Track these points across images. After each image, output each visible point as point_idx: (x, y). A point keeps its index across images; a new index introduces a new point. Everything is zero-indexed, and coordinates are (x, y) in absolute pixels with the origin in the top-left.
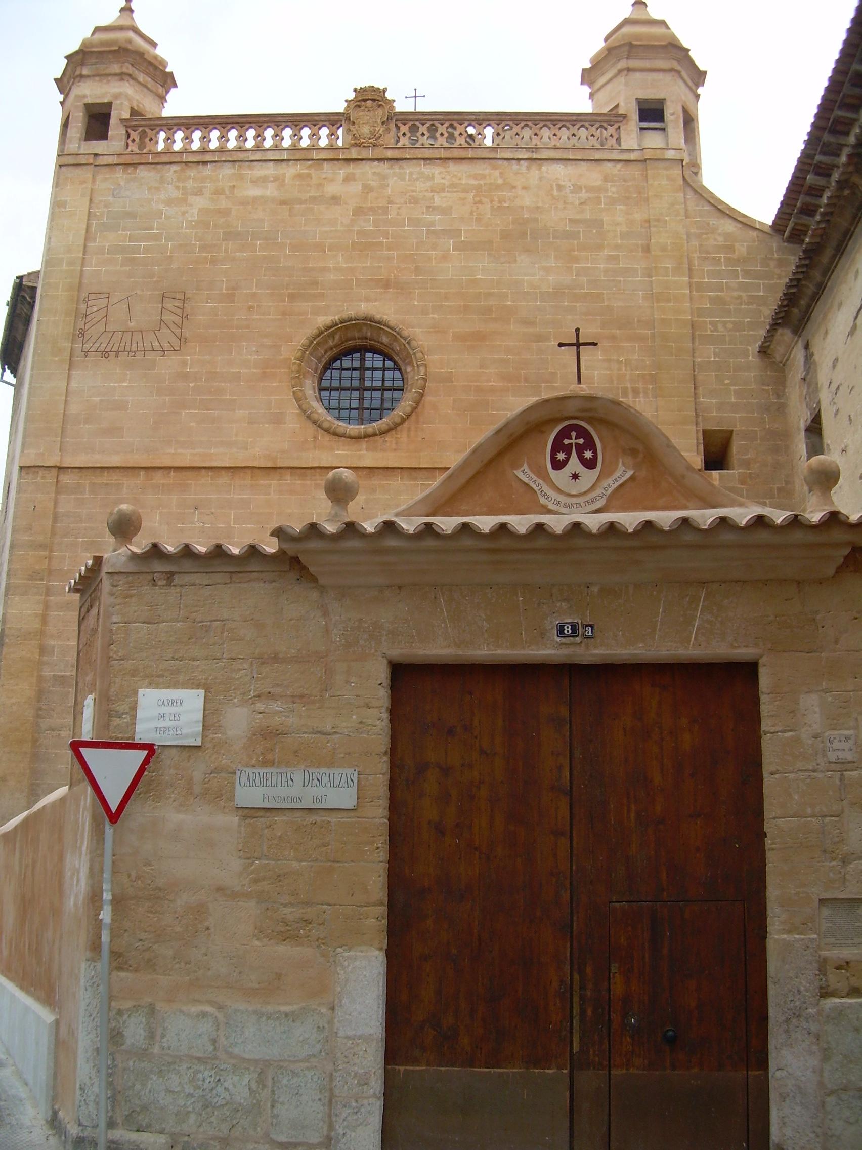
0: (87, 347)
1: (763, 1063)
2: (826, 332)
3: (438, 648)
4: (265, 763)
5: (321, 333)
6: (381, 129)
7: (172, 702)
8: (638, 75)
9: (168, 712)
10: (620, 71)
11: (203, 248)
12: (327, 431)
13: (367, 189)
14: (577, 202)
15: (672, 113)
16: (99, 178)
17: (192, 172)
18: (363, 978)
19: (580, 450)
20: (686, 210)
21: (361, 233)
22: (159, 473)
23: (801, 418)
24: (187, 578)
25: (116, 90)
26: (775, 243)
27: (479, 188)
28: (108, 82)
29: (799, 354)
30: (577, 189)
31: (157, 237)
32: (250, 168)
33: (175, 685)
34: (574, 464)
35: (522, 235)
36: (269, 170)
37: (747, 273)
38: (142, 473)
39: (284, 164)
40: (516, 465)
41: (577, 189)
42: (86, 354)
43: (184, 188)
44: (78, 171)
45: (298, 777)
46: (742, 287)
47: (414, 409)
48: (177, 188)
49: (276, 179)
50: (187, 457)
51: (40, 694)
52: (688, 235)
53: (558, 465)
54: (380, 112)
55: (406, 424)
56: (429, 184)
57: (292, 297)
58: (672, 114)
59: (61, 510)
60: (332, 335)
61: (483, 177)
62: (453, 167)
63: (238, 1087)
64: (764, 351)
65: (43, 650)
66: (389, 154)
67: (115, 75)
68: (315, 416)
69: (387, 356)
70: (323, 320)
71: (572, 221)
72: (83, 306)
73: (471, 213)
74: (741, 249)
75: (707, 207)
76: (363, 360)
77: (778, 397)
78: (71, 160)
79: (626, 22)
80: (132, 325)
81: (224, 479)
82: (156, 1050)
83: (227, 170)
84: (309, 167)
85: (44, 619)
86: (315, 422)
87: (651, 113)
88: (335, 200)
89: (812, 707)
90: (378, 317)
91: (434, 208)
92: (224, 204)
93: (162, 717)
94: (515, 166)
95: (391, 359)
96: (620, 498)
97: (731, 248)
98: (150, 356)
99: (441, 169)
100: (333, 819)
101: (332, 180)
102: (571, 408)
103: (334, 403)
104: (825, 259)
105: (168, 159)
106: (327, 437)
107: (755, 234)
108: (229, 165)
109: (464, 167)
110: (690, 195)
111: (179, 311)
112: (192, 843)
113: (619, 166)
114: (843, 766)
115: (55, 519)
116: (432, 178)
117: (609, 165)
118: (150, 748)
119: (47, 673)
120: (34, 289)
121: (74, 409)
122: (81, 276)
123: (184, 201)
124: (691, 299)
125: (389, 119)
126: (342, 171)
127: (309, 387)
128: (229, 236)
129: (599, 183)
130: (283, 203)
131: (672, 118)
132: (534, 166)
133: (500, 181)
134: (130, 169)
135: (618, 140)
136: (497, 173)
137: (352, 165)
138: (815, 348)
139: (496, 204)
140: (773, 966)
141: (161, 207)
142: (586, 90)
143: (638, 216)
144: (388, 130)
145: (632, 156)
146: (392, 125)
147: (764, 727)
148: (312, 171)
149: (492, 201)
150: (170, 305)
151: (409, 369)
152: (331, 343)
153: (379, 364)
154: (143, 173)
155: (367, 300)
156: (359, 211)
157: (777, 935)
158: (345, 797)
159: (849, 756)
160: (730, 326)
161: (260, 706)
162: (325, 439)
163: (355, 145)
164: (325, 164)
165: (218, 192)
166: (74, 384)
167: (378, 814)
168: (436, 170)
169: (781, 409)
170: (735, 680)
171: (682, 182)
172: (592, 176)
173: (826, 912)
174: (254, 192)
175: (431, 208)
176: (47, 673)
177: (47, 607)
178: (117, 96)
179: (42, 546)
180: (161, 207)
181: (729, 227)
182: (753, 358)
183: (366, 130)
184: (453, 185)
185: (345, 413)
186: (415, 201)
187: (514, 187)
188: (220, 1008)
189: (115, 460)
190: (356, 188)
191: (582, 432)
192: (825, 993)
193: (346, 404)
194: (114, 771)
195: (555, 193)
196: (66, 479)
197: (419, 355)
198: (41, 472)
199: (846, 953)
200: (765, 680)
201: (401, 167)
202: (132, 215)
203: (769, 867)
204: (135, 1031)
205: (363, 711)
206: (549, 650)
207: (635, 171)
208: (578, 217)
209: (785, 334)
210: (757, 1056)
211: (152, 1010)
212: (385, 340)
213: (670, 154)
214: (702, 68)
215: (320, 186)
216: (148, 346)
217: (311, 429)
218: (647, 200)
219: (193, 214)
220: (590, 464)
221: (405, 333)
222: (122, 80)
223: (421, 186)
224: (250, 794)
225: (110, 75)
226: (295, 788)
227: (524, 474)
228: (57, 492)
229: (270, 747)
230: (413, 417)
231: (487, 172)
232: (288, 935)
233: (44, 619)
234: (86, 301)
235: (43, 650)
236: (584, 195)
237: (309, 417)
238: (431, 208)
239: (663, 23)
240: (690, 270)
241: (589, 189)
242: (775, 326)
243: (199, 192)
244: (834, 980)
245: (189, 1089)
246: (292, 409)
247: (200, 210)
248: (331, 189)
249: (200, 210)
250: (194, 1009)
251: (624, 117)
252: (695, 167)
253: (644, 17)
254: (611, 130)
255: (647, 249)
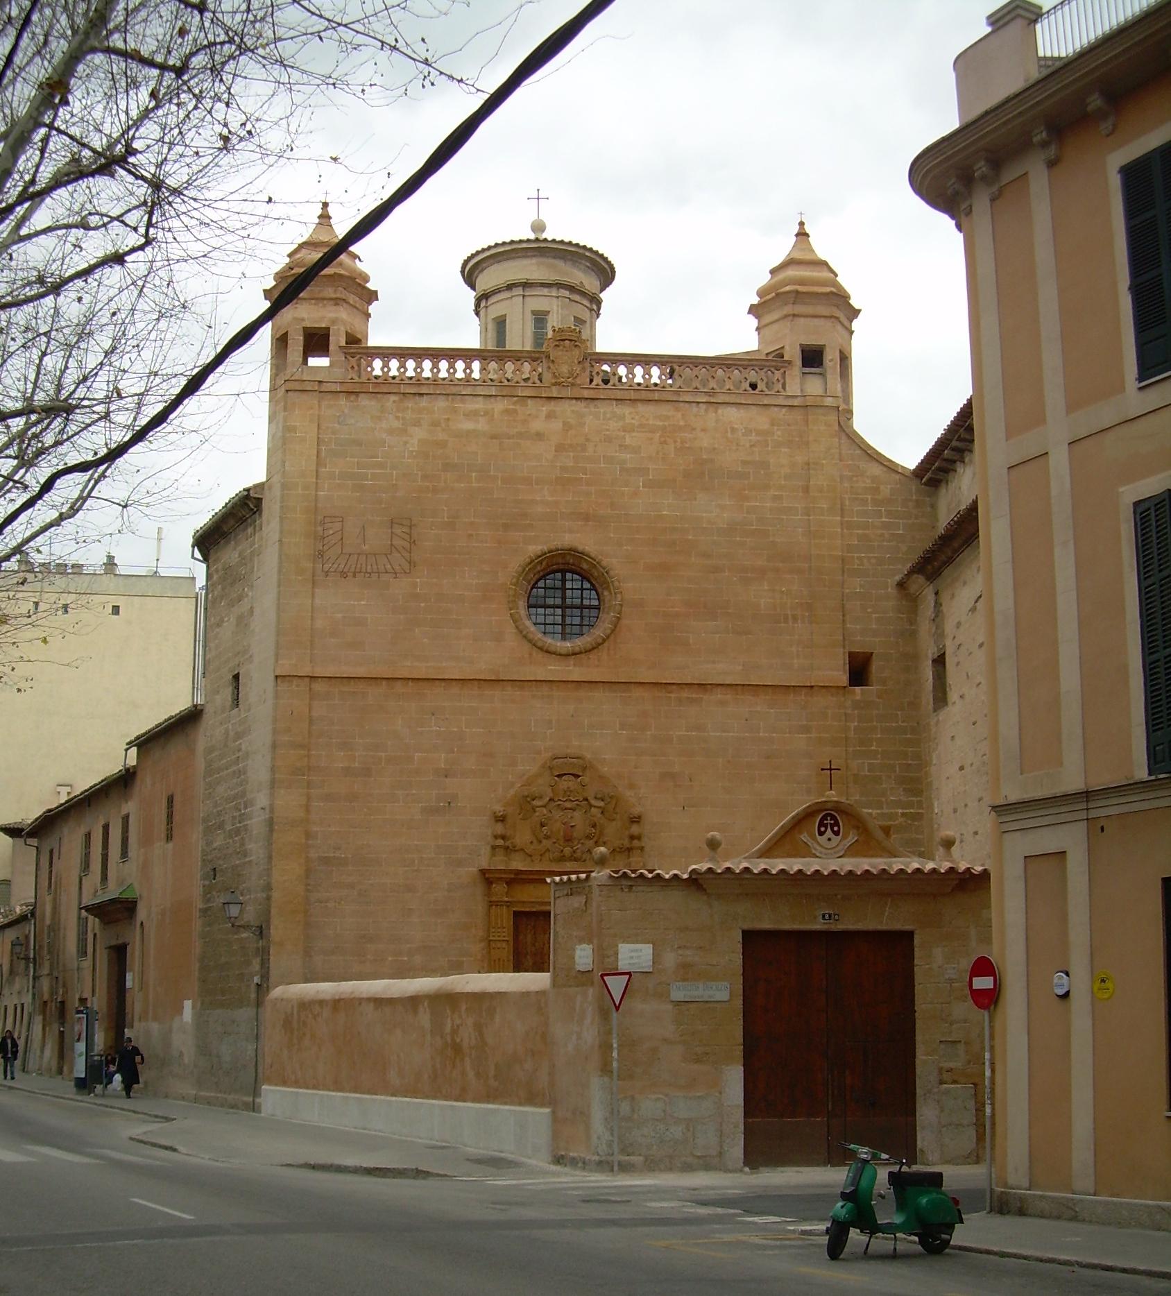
0: (327, 567)
1: (913, 1113)
2: (953, 596)
3: (766, 925)
4: (684, 980)
5: (532, 561)
6: (578, 369)
7: (636, 951)
8: (802, 320)
9: (634, 955)
10: (786, 316)
11: (425, 477)
12: (541, 649)
13: (567, 427)
14: (748, 445)
15: (831, 357)
16: (324, 403)
17: (410, 404)
18: (733, 1080)
19: (832, 826)
20: (840, 454)
21: (563, 469)
22: (399, 683)
23: (931, 652)
24: (640, 888)
25: (332, 315)
26: (914, 485)
27: (664, 428)
28: (325, 306)
29: (929, 594)
30: (748, 432)
31: (381, 466)
32: (463, 402)
33: (637, 942)
34: (829, 833)
35: (700, 475)
36: (479, 404)
37: (889, 514)
38: (384, 682)
39: (492, 399)
40: (800, 833)
41: (748, 432)
42: (327, 574)
43: (403, 418)
44: (304, 397)
45: (701, 986)
46: (886, 526)
47: (613, 631)
48: (397, 418)
49: (486, 413)
50: (422, 670)
51: (308, 872)
52: (842, 477)
53: (821, 834)
54: (576, 352)
55: (606, 644)
56: (620, 424)
57: (506, 527)
58: (831, 360)
59: (314, 714)
60: (541, 562)
61: (667, 417)
62: (641, 408)
63: (677, 1131)
64: (901, 585)
65: (308, 835)
66: (586, 394)
67: (331, 299)
68: (531, 636)
69: (584, 578)
70: (535, 549)
71: (744, 463)
72: (320, 529)
73: (658, 453)
74: (886, 490)
75: (858, 452)
76: (564, 580)
77: (911, 624)
78: (297, 386)
79: (789, 263)
80: (366, 548)
81: (455, 689)
82: (636, 1116)
83: (441, 403)
84: (515, 403)
85: (307, 809)
86: (530, 641)
87: (812, 358)
88: (539, 436)
89: (938, 953)
90: (580, 548)
91: (626, 447)
92: (441, 436)
93: (632, 958)
94: (694, 408)
95: (589, 581)
96: (851, 852)
97: (876, 490)
98: (385, 577)
99: (632, 410)
100: (718, 1006)
101: (537, 417)
102: (829, 806)
103: (541, 619)
104: (956, 544)
105: (384, 387)
106: (541, 655)
107: (897, 477)
108: (443, 398)
109: (651, 408)
110: (844, 439)
111: (407, 537)
112: (650, 1019)
113: (784, 410)
114: (951, 981)
115: (311, 722)
116: (622, 418)
117: (776, 409)
118: (629, 974)
119: (313, 854)
120: (259, 500)
121: (319, 624)
122: (316, 500)
123: (404, 431)
124: (842, 536)
125: (585, 358)
126: (545, 408)
127: (522, 604)
128: (447, 467)
129: (766, 427)
130: (493, 437)
131: (831, 364)
132: (711, 409)
133: (682, 423)
134: (353, 397)
135: (784, 387)
136: (679, 415)
137: (553, 403)
138: (945, 598)
139: (679, 445)
140: (918, 1071)
141: (384, 436)
142: (753, 322)
143: (800, 459)
144: (584, 369)
145: (796, 402)
146: (587, 364)
147: (916, 962)
148: (518, 407)
149: (675, 442)
150: (398, 530)
151: (606, 593)
152: (539, 568)
153: (577, 585)
154: (364, 401)
155: (571, 531)
156: (560, 448)
157: (920, 1056)
158: (723, 995)
159: (954, 977)
160: (873, 561)
161: (680, 952)
162: (539, 656)
163: (556, 384)
164: (529, 401)
165: (435, 424)
166: (317, 601)
167: (739, 1002)
168: (626, 410)
169: (913, 635)
170: (904, 939)
171: (837, 428)
172: (761, 420)
173: (942, 1046)
174: (468, 425)
175: (623, 447)
176: (313, 854)
177: (309, 798)
178: (334, 321)
179: (301, 746)
180: (384, 436)
181: (876, 470)
182: (892, 590)
183: (565, 369)
184: (641, 426)
185: (549, 628)
186: (609, 439)
187: (694, 429)
188: (667, 1095)
189: (361, 671)
190: (557, 425)
191: (833, 817)
192: (941, 1082)
193: (550, 620)
194: (616, 985)
195: (729, 435)
196: (318, 687)
197: (616, 584)
198: (295, 681)
199: (951, 1065)
200: (917, 940)
201: (596, 406)
202: (358, 443)
203: (917, 1026)
204: (625, 1107)
205: (731, 956)
206: (819, 925)
207: (798, 416)
208: (749, 458)
209: (920, 579)
210: (910, 1110)
211: (633, 1098)
212: (585, 566)
213: (829, 401)
214: (857, 307)
215: (525, 422)
216: (382, 569)
217: (527, 646)
218: (808, 443)
219: (414, 445)
220: (837, 833)
221: (604, 563)
222: (337, 304)
223: (614, 425)
224: (678, 994)
225: (324, 299)
226: (699, 991)
227: (804, 837)
228: (311, 699)
229: (686, 972)
230: (612, 637)
231: (670, 414)
232: (698, 1061)
233: (307, 809)
234: (322, 523)
235: (308, 835)
236: (753, 437)
237: (525, 637)
238: (623, 447)
239: (824, 264)
240: (842, 510)
241: (759, 433)
242: (911, 572)
243: (417, 423)
244: (946, 1076)
245: (653, 1134)
246: (510, 629)
247: (419, 440)
248: (537, 425)
249: (419, 440)
250: (654, 1097)
251: (789, 362)
252: (847, 413)
253: (808, 257)
254: (778, 374)
255: (806, 489)
